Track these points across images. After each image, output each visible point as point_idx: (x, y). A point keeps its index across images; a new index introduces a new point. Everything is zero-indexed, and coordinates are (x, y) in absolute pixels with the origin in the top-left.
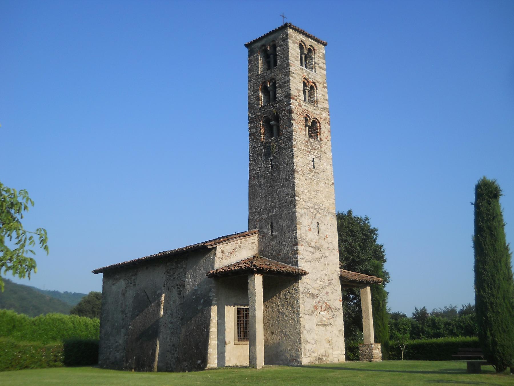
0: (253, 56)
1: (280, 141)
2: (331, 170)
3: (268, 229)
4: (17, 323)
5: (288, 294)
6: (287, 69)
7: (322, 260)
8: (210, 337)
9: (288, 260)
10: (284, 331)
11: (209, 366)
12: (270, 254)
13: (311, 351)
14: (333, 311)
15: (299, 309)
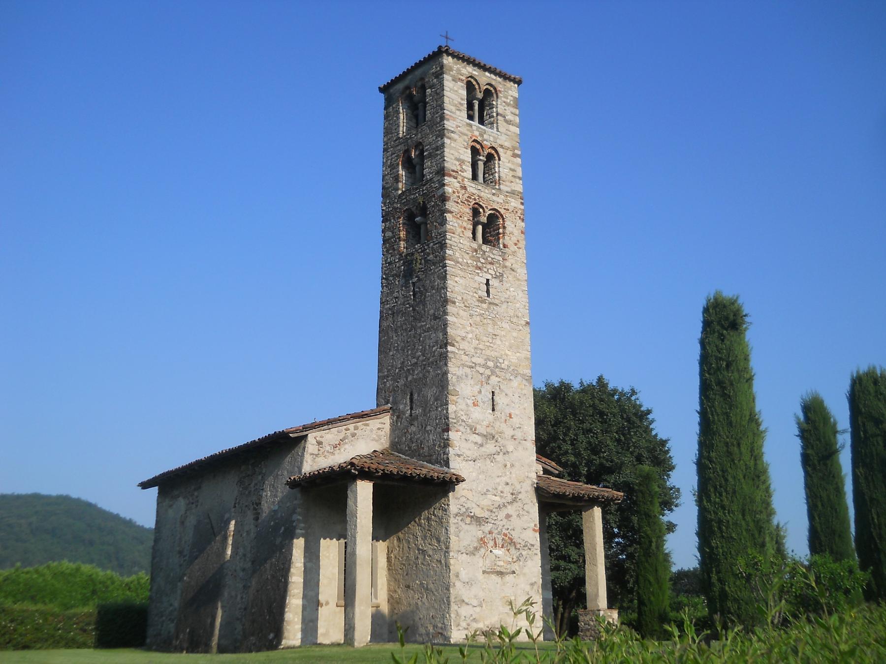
0: (391, 107)
1: (428, 251)
2: (523, 299)
3: (406, 404)
6: (440, 126)
7: (499, 458)
8: (289, 593)
11: (285, 643)
12: (407, 448)
14: (519, 549)
15: (449, 543)
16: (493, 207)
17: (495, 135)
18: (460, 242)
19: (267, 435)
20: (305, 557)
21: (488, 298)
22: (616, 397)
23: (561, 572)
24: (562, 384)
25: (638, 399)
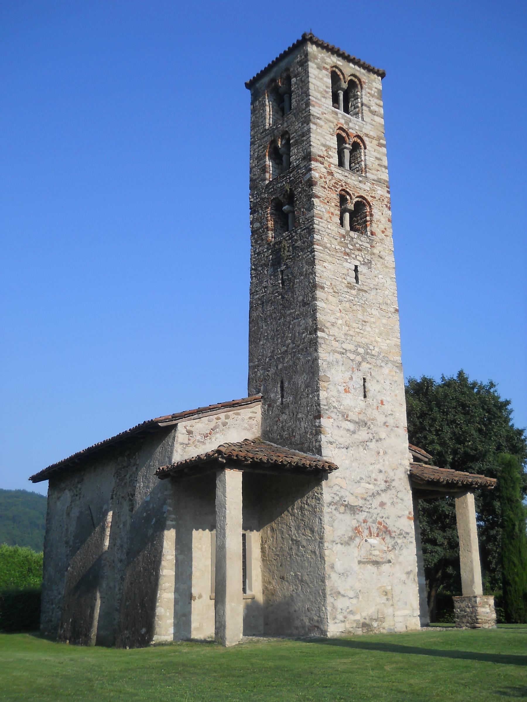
1: (295, 237)
2: (392, 287)
4: (33, 565)
5: (306, 506)
6: (306, 112)
7: (372, 445)
8: (160, 587)
9: (306, 445)
10: (300, 574)
11: (156, 638)
13: (346, 611)
15: (323, 534)
16: (360, 195)
17: (360, 124)
18: (328, 227)
19: (137, 425)
20: (176, 549)
21: (356, 285)
22: (475, 390)
23: (428, 555)
24: (424, 379)
25: (496, 391)
